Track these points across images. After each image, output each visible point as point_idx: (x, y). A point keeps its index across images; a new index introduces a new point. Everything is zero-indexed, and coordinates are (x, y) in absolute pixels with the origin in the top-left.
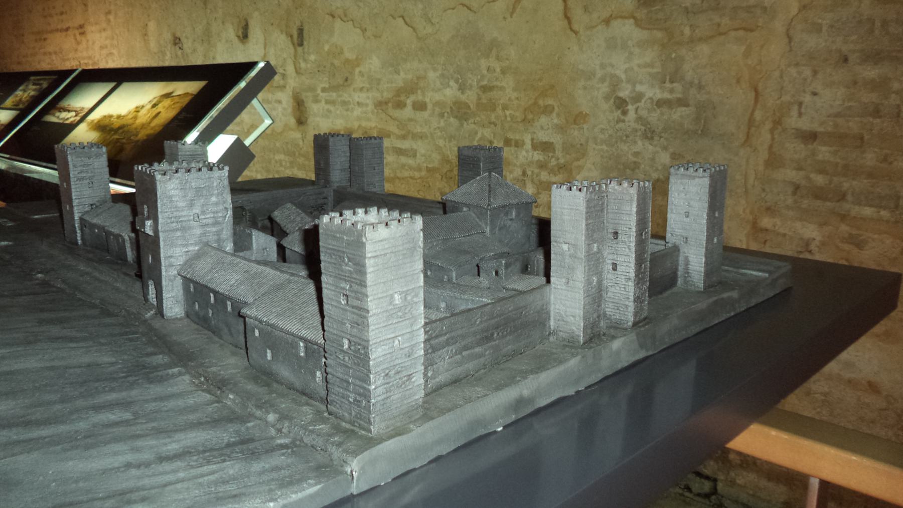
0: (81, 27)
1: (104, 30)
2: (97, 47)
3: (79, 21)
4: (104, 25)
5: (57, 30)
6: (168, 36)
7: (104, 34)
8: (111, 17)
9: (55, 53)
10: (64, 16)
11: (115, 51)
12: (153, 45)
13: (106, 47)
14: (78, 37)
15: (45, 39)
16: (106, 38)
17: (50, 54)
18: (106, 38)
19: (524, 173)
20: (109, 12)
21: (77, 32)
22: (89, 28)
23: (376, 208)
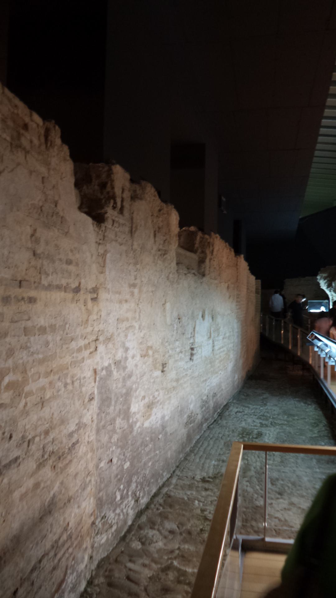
0: (95, 290)
1: (126, 301)
2: (112, 320)
3: (89, 283)
4: (128, 297)
5: (59, 287)
6: (175, 314)
7: (125, 306)
8: (136, 291)
9: (53, 328)
10: (71, 268)
11: (136, 325)
12: (168, 320)
13: (127, 319)
14: (90, 303)
15: (32, 300)
16: (128, 310)
17: (43, 330)
18: (128, 310)
19: (181, 352)
20: (134, 286)
21: (89, 296)
22: (103, 295)
23: (331, 322)
